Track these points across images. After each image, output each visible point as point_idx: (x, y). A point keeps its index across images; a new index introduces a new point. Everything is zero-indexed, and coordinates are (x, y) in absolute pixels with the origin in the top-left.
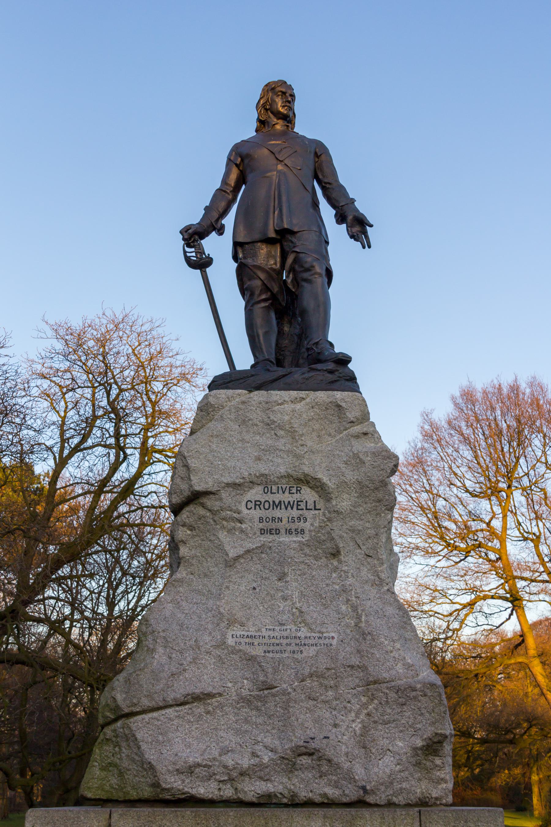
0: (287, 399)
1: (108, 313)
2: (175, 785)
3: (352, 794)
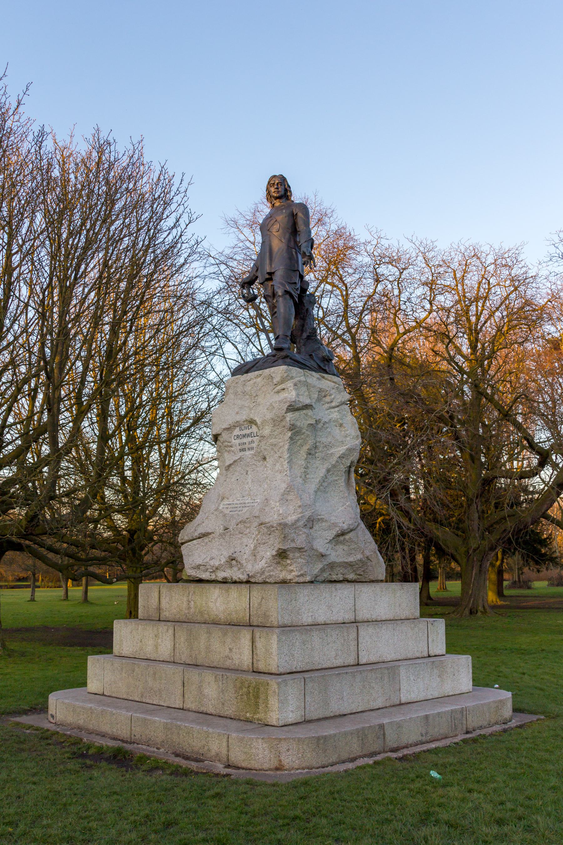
1: (435, 244)
3: (244, 577)
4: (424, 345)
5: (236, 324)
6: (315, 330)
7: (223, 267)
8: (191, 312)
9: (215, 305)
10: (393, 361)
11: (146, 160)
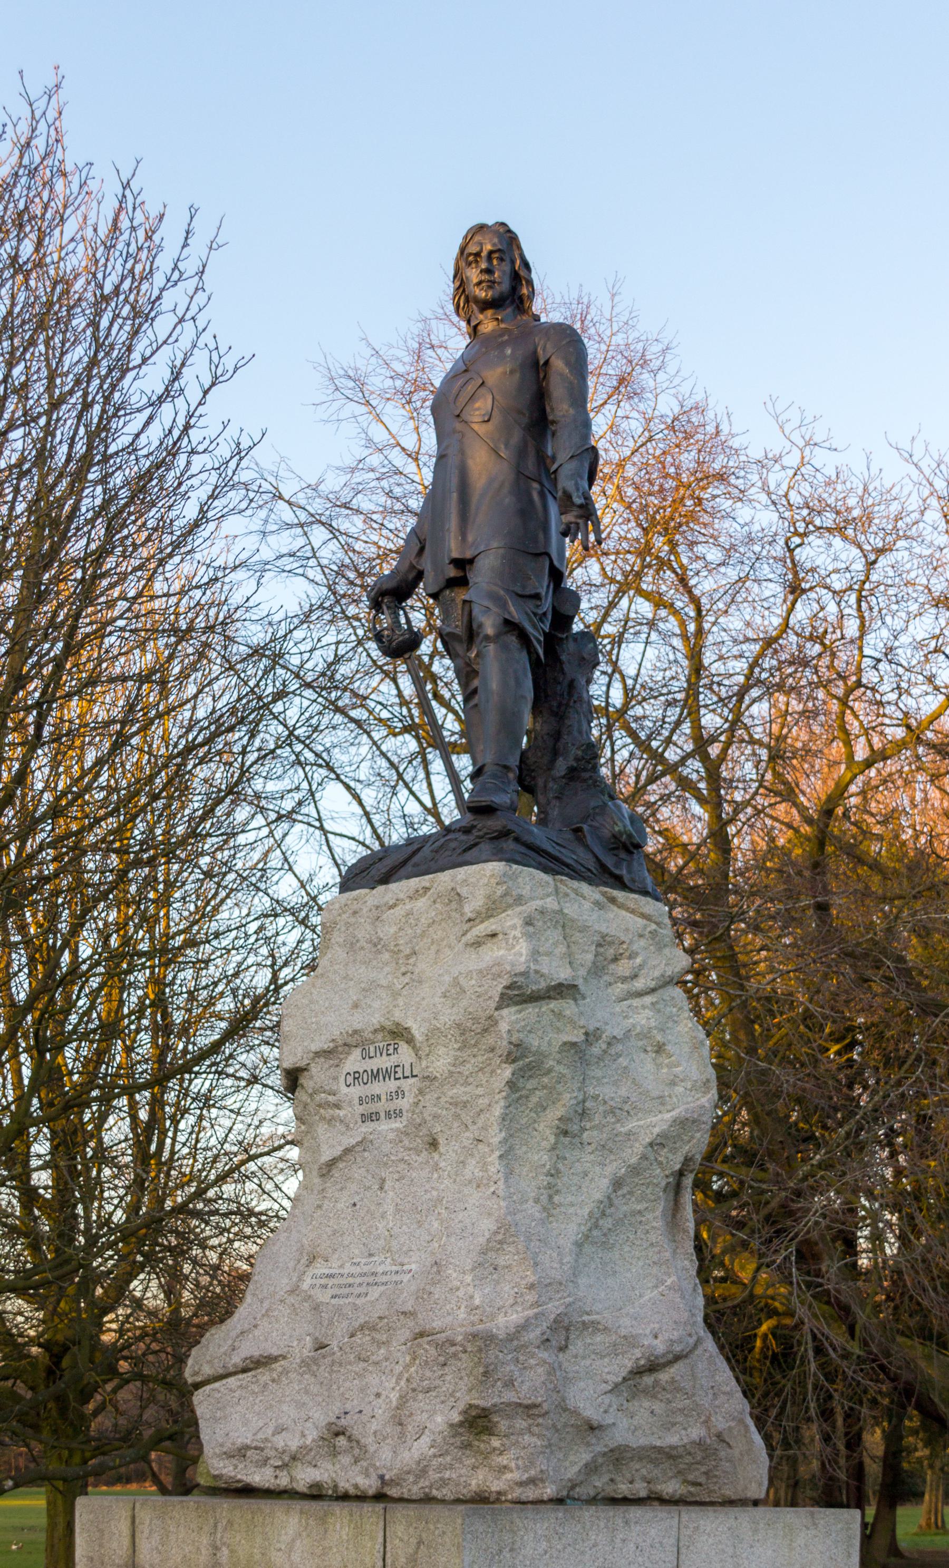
0: (401, 896)
2: (224, 1471)
3: (369, 1484)
4: (926, 800)
5: (358, 723)
6: (591, 752)
7: (319, 534)
8: (222, 682)
9: (295, 661)
10: (830, 849)
11: (72, 157)
